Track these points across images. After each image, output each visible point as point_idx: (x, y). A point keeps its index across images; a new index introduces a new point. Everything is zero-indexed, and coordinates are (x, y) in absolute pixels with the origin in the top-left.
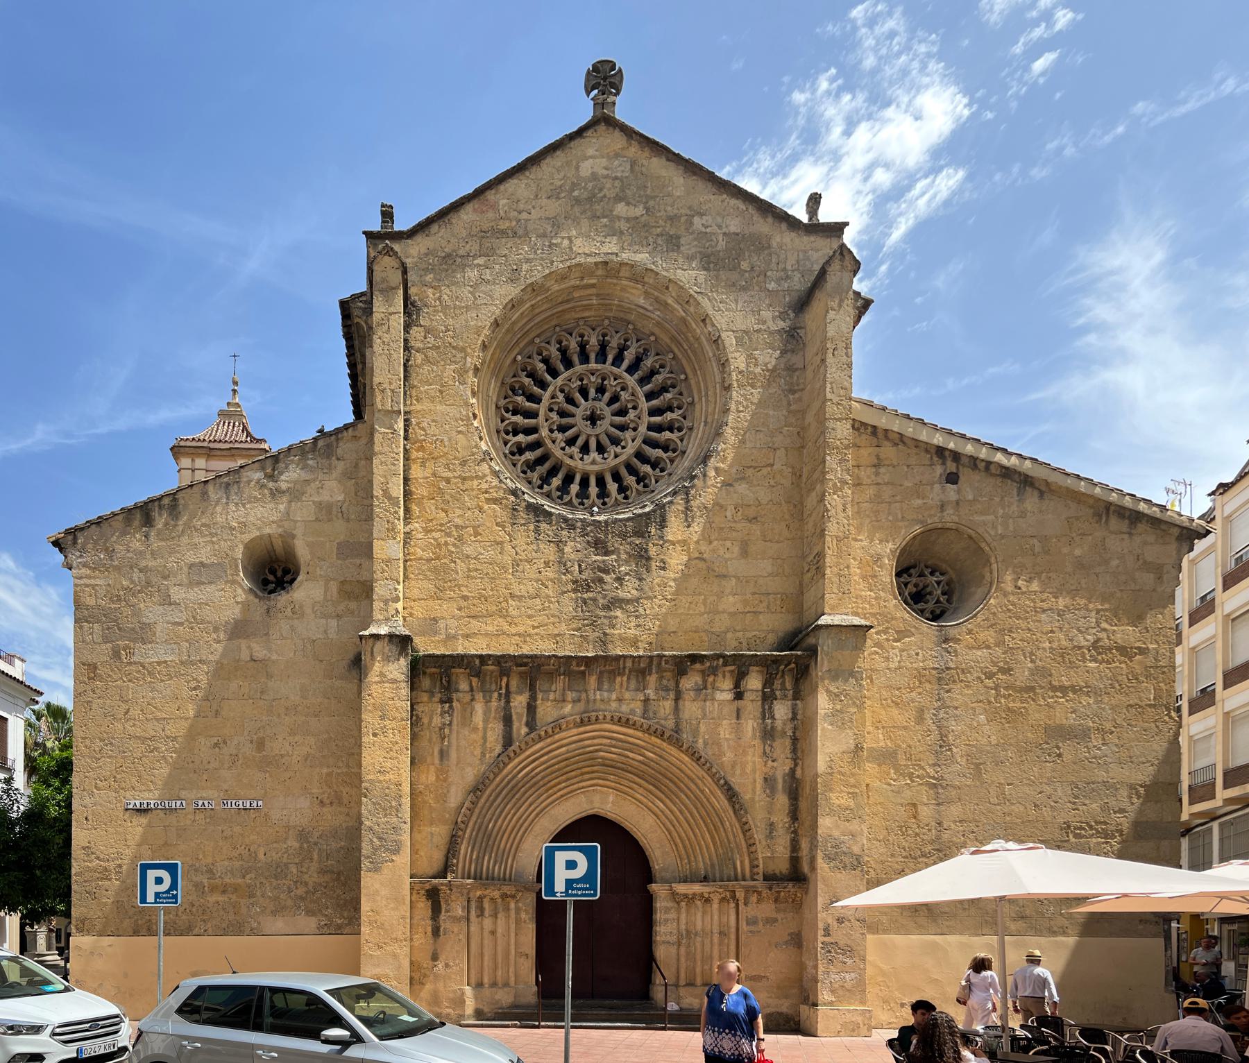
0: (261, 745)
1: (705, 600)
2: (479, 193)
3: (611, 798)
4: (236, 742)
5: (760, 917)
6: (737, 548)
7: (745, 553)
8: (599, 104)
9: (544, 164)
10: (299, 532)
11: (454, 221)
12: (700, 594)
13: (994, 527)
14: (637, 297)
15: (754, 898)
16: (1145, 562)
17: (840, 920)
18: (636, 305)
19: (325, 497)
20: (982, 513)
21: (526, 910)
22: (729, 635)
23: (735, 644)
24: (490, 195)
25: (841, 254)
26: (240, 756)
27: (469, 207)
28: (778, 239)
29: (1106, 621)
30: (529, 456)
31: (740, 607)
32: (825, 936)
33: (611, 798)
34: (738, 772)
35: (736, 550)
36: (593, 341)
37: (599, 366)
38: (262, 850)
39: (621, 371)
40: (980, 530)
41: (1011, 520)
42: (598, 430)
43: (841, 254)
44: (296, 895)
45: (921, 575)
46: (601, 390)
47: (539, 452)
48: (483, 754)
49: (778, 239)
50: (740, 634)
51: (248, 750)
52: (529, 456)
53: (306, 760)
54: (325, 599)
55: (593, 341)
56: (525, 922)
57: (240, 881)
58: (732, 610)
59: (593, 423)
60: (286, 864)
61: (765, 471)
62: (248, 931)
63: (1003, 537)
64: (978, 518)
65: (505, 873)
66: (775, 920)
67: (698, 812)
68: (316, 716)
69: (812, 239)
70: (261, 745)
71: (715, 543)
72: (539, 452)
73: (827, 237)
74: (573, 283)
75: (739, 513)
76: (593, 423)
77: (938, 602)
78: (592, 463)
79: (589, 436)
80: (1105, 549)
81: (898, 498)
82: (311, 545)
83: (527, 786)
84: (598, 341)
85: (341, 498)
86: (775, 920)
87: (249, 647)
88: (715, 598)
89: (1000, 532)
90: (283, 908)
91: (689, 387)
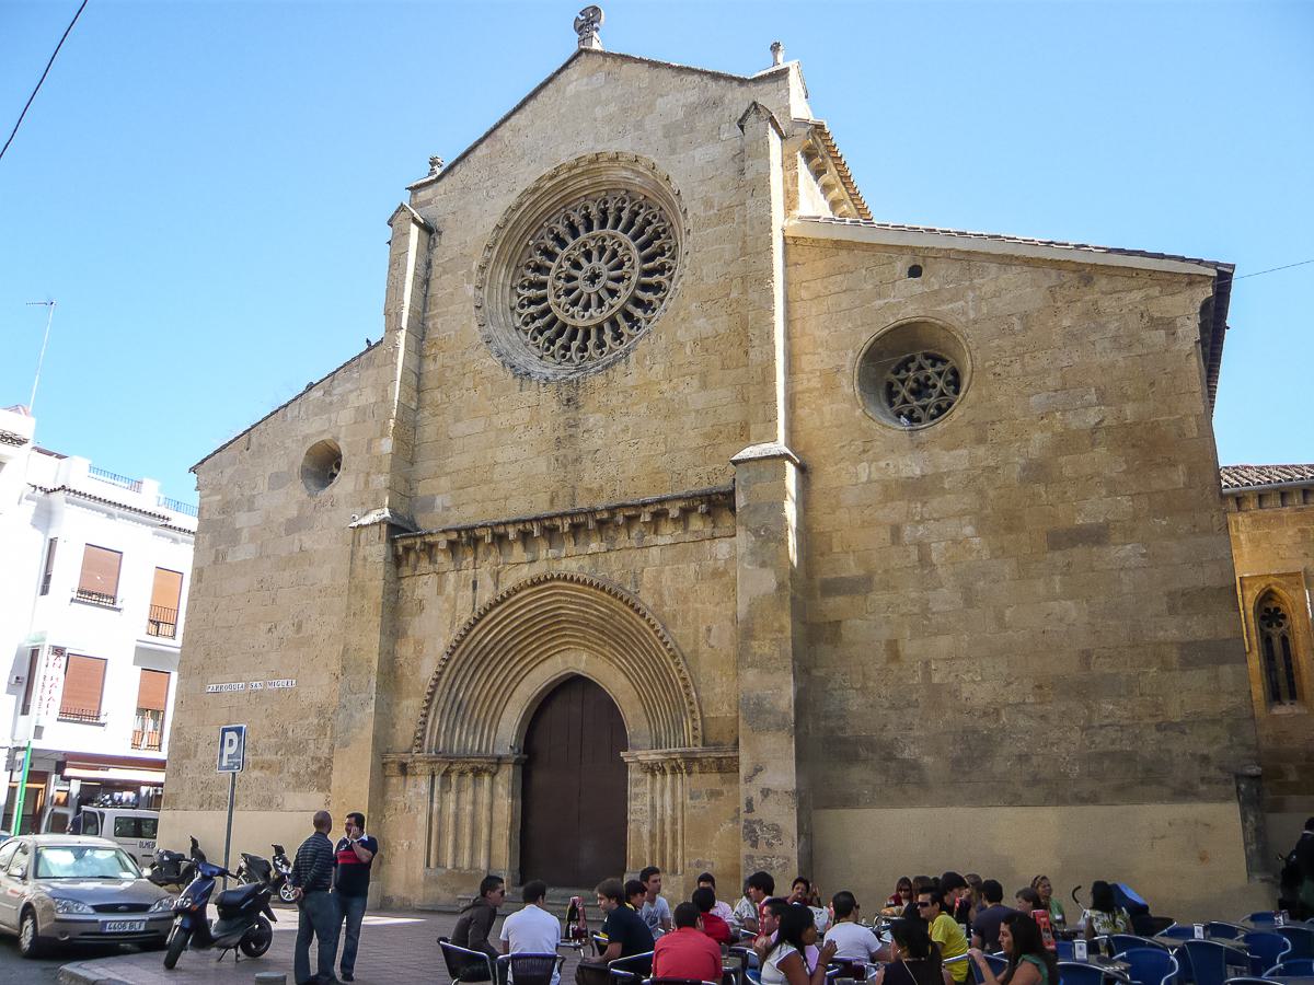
0: (299, 627)
3: (584, 657)
6: (696, 381)
7: (704, 386)
9: (539, 97)
13: (964, 313)
14: (619, 174)
15: (696, 768)
16: (1152, 319)
17: (766, 793)
19: (362, 401)
20: (951, 301)
21: (503, 785)
22: (690, 472)
24: (499, 132)
25: (756, 108)
30: (539, 323)
31: (700, 441)
33: (584, 657)
34: (680, 622)
35: (695, 383)
36: (594, 210)
37: (558, 260)
38: (291, 727)
43: (756, 108)
45: (921, 368)
48: (452, 623)
49: (730, 96)
51: (290, 632)
52: (539, 323)
54: (355, 491)
56: (502, 797)
57: (274, 757)
59: (593, 282)
62: (275, 807)
63: (975, 322)
64: (945, 308)
65: (473, 746)
66: (720, 793)
67: (511, 681)
68: (340, 596)
69: (760, 87)
73: (774, 82)
76: (593, 282)
78: (597, 315)
80: (1099, 313)
81: (857, 303)
84: (540, 255)
86: (720, 793)
87: (300, 540)
89: (972, 317)
91: (674, 232)
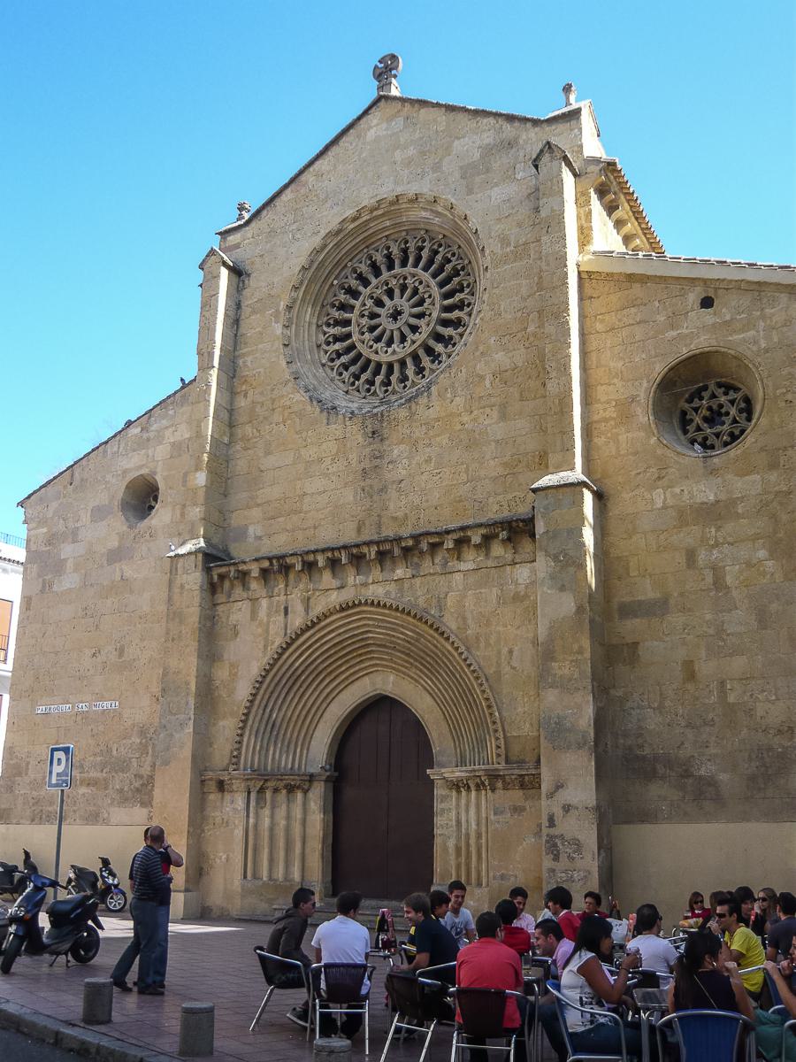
0: (121, 652)
1: (467, 468)
2: (292, 180)
4: (106, 651)
5: (506, 806)
7: (504, 416)
8: (380, 88)
9: (341, 143)
10: (159, 470)
11: (277, 204)
12: (462, 464)
13: (756, 342)
15: (499, 784)
18: (421, 218)
23: (496, 507)
24: (303, 178)
26: (108, 663)
27: (288, 191)
28: (524, 137)
29: (421, 583)
31: (500, 470)
32: (550, 827)
34: (482, 645)
36: (395, 250)
37: (361, 298)
39: (419, 271)
40: (740, 349)
41: (774, 332)
42: (399, 324)
43: (550, 147)
44: (134, 787)
46: (404, 288)
47: (352, 354)
48: (265, 647)
49: (524, 137)
50: (500, 498)
52: (344, 359)
53: (149, 663)
54: (172, 522)
55: (395, 250)
58: (494, 474)
59: (400, 313)
60: (130, 758)
61: (519, 335)
63: (767, 351)
69: (554, 127)
70: (121, 652)
71: (475, 412)
72: (352, 354)
73: (567, 122)
74: (364, 219)
75: (497, 380)
77: (735, 421)
79: (392, 331)
82: (165, 479)
83: (307, 673)
85: (187, 436)
86: (523, 809)
87: (121, 570)
88: (477, 465)
89: (763, 346)
90: (126, 799)
